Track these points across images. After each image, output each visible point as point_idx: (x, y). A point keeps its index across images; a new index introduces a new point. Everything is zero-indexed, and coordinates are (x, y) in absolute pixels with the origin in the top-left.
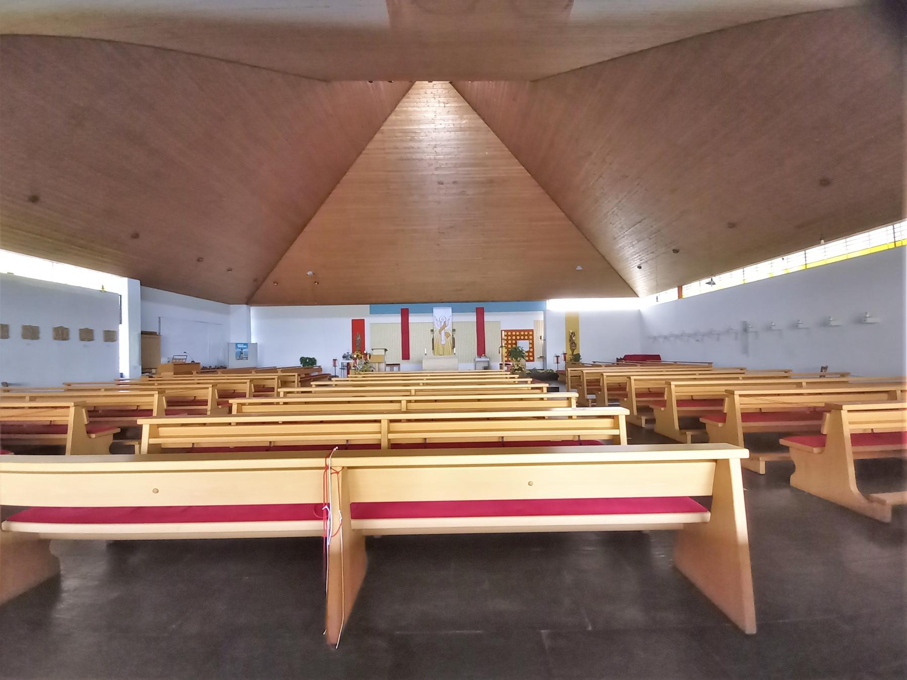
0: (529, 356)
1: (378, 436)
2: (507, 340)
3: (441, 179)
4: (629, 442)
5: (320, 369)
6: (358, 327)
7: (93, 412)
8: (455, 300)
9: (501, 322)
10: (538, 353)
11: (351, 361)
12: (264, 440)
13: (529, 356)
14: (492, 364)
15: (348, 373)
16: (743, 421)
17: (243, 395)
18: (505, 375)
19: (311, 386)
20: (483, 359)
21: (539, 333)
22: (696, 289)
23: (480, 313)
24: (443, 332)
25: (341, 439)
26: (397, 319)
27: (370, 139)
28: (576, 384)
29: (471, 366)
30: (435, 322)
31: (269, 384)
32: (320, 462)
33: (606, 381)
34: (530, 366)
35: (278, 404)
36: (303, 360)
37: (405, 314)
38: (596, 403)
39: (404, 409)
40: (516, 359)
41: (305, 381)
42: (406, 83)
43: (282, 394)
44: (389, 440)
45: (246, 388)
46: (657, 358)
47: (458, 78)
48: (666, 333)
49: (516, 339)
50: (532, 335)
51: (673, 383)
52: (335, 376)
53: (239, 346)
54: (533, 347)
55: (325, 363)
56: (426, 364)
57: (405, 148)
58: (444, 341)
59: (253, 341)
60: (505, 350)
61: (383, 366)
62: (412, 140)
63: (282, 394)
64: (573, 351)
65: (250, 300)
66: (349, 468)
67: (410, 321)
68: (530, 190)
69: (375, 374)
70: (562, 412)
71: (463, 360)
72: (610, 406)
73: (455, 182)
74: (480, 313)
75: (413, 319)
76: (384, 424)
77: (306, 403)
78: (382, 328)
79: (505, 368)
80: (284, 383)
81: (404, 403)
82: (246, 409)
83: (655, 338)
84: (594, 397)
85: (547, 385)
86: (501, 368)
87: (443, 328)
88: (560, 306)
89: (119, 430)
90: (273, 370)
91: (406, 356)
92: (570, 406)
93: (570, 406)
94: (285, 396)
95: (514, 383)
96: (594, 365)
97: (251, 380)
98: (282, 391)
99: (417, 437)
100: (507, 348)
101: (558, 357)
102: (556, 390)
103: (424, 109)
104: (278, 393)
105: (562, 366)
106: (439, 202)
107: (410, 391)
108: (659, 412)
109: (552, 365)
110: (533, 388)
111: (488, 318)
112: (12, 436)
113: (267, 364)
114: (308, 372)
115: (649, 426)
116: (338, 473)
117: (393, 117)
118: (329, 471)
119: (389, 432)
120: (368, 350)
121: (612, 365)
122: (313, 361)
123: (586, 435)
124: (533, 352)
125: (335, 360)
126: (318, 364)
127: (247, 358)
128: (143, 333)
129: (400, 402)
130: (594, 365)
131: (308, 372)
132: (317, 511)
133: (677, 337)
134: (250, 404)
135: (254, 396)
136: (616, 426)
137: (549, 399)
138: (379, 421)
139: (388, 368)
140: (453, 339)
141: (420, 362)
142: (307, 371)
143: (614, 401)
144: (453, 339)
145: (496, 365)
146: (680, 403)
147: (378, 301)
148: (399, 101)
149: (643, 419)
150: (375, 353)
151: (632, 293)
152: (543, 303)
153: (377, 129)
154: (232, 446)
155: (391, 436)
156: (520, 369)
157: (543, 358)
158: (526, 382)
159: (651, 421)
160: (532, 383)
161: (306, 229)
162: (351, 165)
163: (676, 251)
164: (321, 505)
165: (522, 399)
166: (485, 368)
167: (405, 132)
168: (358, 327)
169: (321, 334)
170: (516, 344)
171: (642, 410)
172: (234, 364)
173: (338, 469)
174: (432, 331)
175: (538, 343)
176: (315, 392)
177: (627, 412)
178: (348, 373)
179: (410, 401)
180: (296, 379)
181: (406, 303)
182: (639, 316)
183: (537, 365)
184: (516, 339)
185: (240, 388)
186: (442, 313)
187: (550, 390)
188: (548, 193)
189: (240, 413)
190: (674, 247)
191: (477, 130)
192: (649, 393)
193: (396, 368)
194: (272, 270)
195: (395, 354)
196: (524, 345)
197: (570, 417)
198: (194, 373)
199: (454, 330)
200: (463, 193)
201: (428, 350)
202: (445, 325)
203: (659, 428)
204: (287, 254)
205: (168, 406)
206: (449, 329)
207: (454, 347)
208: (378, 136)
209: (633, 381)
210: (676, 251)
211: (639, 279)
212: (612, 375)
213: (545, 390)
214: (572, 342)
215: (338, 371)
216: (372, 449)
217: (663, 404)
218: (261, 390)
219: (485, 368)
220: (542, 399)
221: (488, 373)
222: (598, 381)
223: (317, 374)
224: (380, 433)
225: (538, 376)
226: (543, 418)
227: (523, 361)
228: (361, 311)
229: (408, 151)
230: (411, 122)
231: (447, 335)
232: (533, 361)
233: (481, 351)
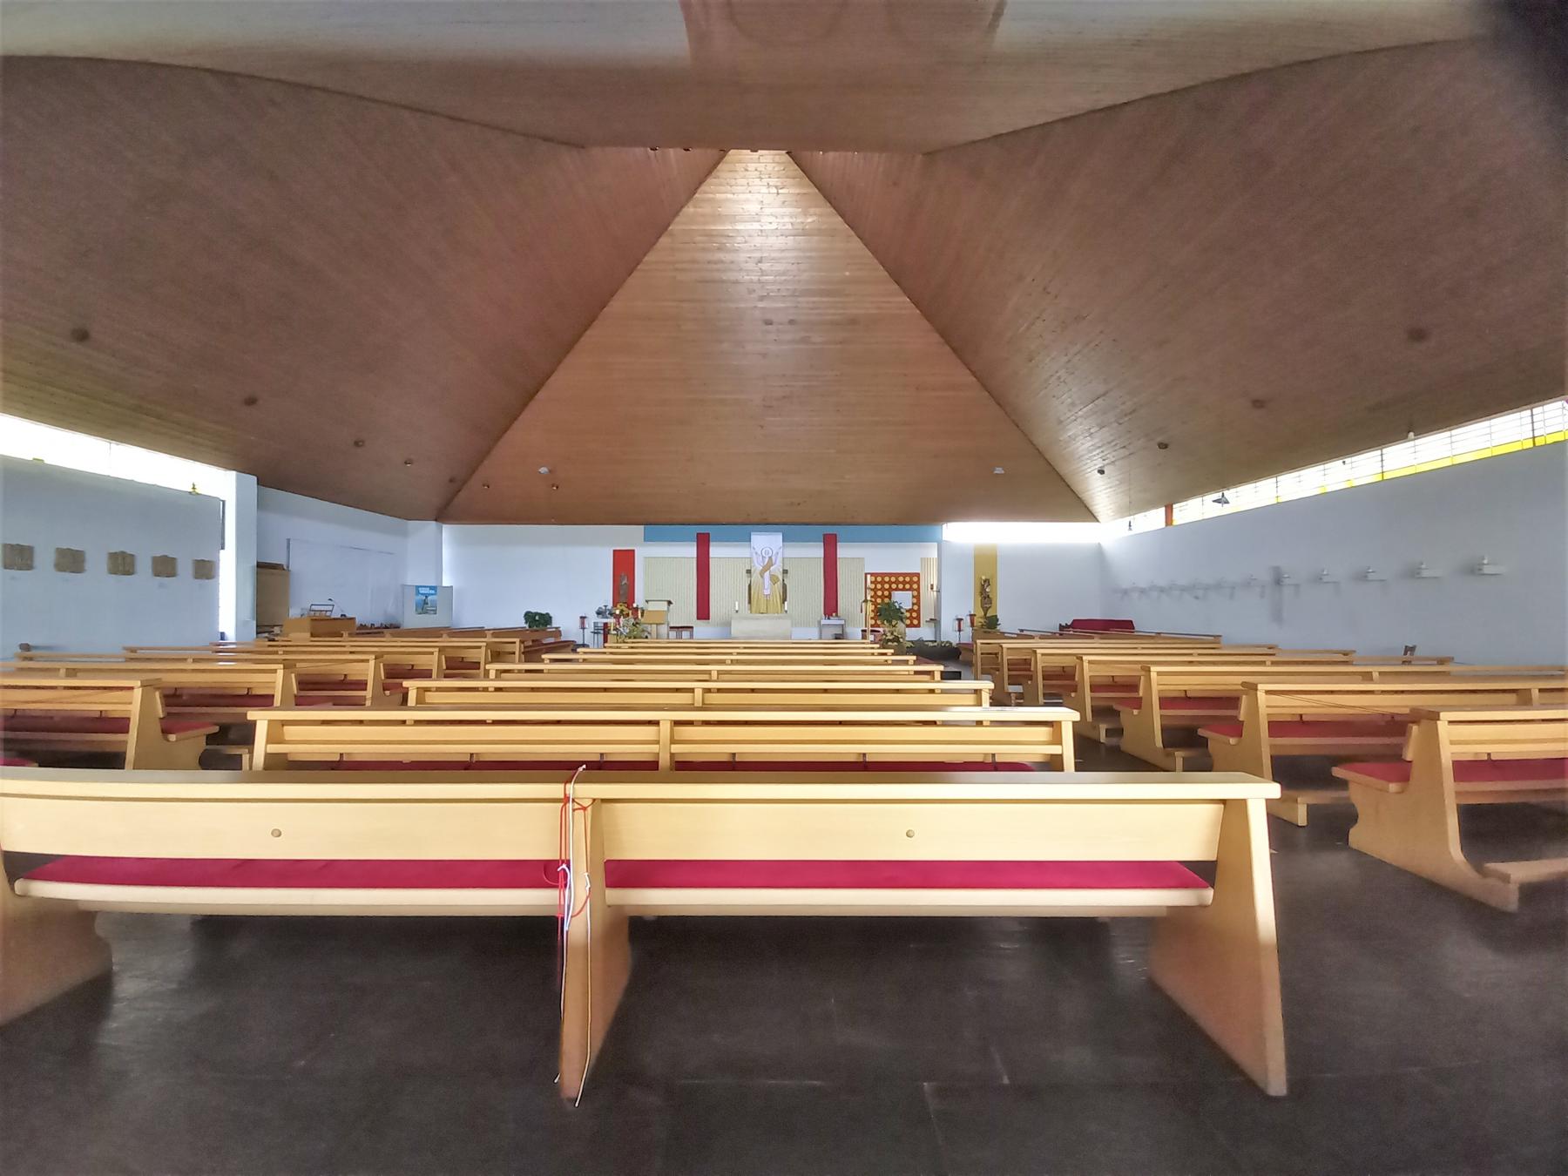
0: (911, 618)
1: (655, 748)
2: (875, 590)
3: (768, 316)
4: (1078, 768)
5: (558, 632)
6: (624, 563)
7: (173, 698)
8: (790, 523)
9: (865, 559)
10: (926, 614)
11: (611, 621)
12: (460, 751)
13: (911, 618)
14: (848, 630)
15: (605, 641)
16: (1271, 735)
17: (426, 674)
18: (870, 649)
19: (542, 661)
20: (833, 621)
21: (930, 578)
22: (1196, 510)
23: (830, 544)
25: (592, 752)
26: (691, 551)
28: (990, 668)
29: (812, 634)
30: (754, 557)
31: (471, 656)
32: (555, 790)
33: (1041, 663)
34: (912, 634)
35: (485, 689)
36: (530, 617)
37: (703, 543)
38: (1023, 700)
39: (698, 703)
40: (890, 622)
41: (532, 653)
43: (492, 674)
44: (672, 755)
45: (432, 661)
48: (1143, 585)
49: (890, 589)
50: (918, 583)
51: (1153, 669)
52: (584, 645)
53: (422, 591)
54: (918, 604)
55: (566, 623)
56: (738, 628)
58: (767, 588)
59: (445, 584)
60: (870, 607)
61: (664, 629)
63: (492, 674)
65: (443, 515)
66: (604, 801)
68: (920, 338)
69: (651, 642)
70: (966, 714)
71: (801, 622)
72: (1046, 705)
73: (792, 322)
74: (830, 544)
75: (715, 551)
76: (665, 728)
77: (533, 690)
78: (665, 566)
79: (871, 637)
80: (497, 656)
81: (698, 693)
82: (431, 697)
83: (1125, 592)
84: (1019, 689)
85: (941, 668)
86: (864, 637)
87: (766, 568)
88: (965, 534)
89: (216, 729)
90: (479, 632)
91: (703, 612)
92: (979, 704)
93: (979, 704)
95: (886, 663)
96: (1022, 635)
97: (442, 650)
98: (493, 668)
99: (721, 752)
100: (875, 603)
101: (960, 620)
102: (957, 676)
103: (742, 197)
104: (487, 672)
105: (967, 636)
106: (764, 355)
107: (709, 672)
108: (1129, 717)
109: (950, 635)
110: (916, 673)
111: (844, 552)
113: (468, 622)
114: (538, 637)
115: (1114, 741)
116: (585, 809)
117: (689, 209)
118: (570, 805)
119: (673, 741)
120: (639, 601)
121: (1052, 636)
122: (546, 619)
123: (1005, 753)
124: (918, 612)
125: (583, 618)
128: (260, 565)
129: (692, 690)
130: (1022, 635)
131: (538, 637)
133: (1162, 590)
134: (439, 689)
135: (446, 676)
136: (1057, 740)
137: (944, 692)
138: (656, 723)
139: (673, 634)
140: (784, 587)
141: (728, 624)
142: (536, 636)
143: (1053, 699)
144: (784, 587)
145: (855, 631)
146: (1166, 702)
147: (658, 519)
148: (701, 183)
149: (1103, 728)
150: (651, 607)
151: (1090, 515)
152: (937, 528)
153: (663, 229)
154: (406, 759)
155: (676, 748)
156: (896, 639)
157: (935, 621)
158: (906, 662)
159: (1116, 732)
160: (915, 663)
161: (541, 395)
163: (1163, 446)
164: (556, 863)
165: (898, 691)
166: (837, 637)
167: (709, 235)
168: (624, 563)
169: (564, 576)
170: (890, 597)
171: (1101, 712)
172: (412, 620)
173: (587, 803)
174: (749, 572)
175: (928, 597)
176: (550, 672)
177: (1076, 716)
178: (605, 641)
179: (708, 690)
180: (517, 648)
181: (705, 524)
183: (925, 633)
184: (890, 589)
185: (422, 662)
186: (766, 543)
187: (945, 676)
189: (421, 704)
190: (1159, 439)
191: (832, 233)
192: (1114, 685)
193: (685, 634)
195: (685, 611)
196: (903, 599)
197: (979, 723)
198: (345, 634)
199: (785, 572)
200: (805, 340)
201: (740, 603)
202: (770, 563)
203: (1127, 744)
205: (300, 689)
206: (777, 570)
207: (784, 600)
208: (664, 241)
209: (1086, 664)
210: (1163, 446)
211: (1100, 491)
212: (1050, 653)
213: (938, 676)
214: (985, 595)
215: (588, 637)
216: (643, 769)
217: (1137, 703)
218: (458, 666)
219: (837, 637)
220: (932, 691)
221: (841, 646)
222: (1027, 662)
223: (552, 640)
224: (657, 742)
225: (925, 652)
226: (934, 723)
227: (901, 626)
228: (629, 536)
230: (719, 218)
231: (774, 579)
232: (918, 626)
233: (831, 607)
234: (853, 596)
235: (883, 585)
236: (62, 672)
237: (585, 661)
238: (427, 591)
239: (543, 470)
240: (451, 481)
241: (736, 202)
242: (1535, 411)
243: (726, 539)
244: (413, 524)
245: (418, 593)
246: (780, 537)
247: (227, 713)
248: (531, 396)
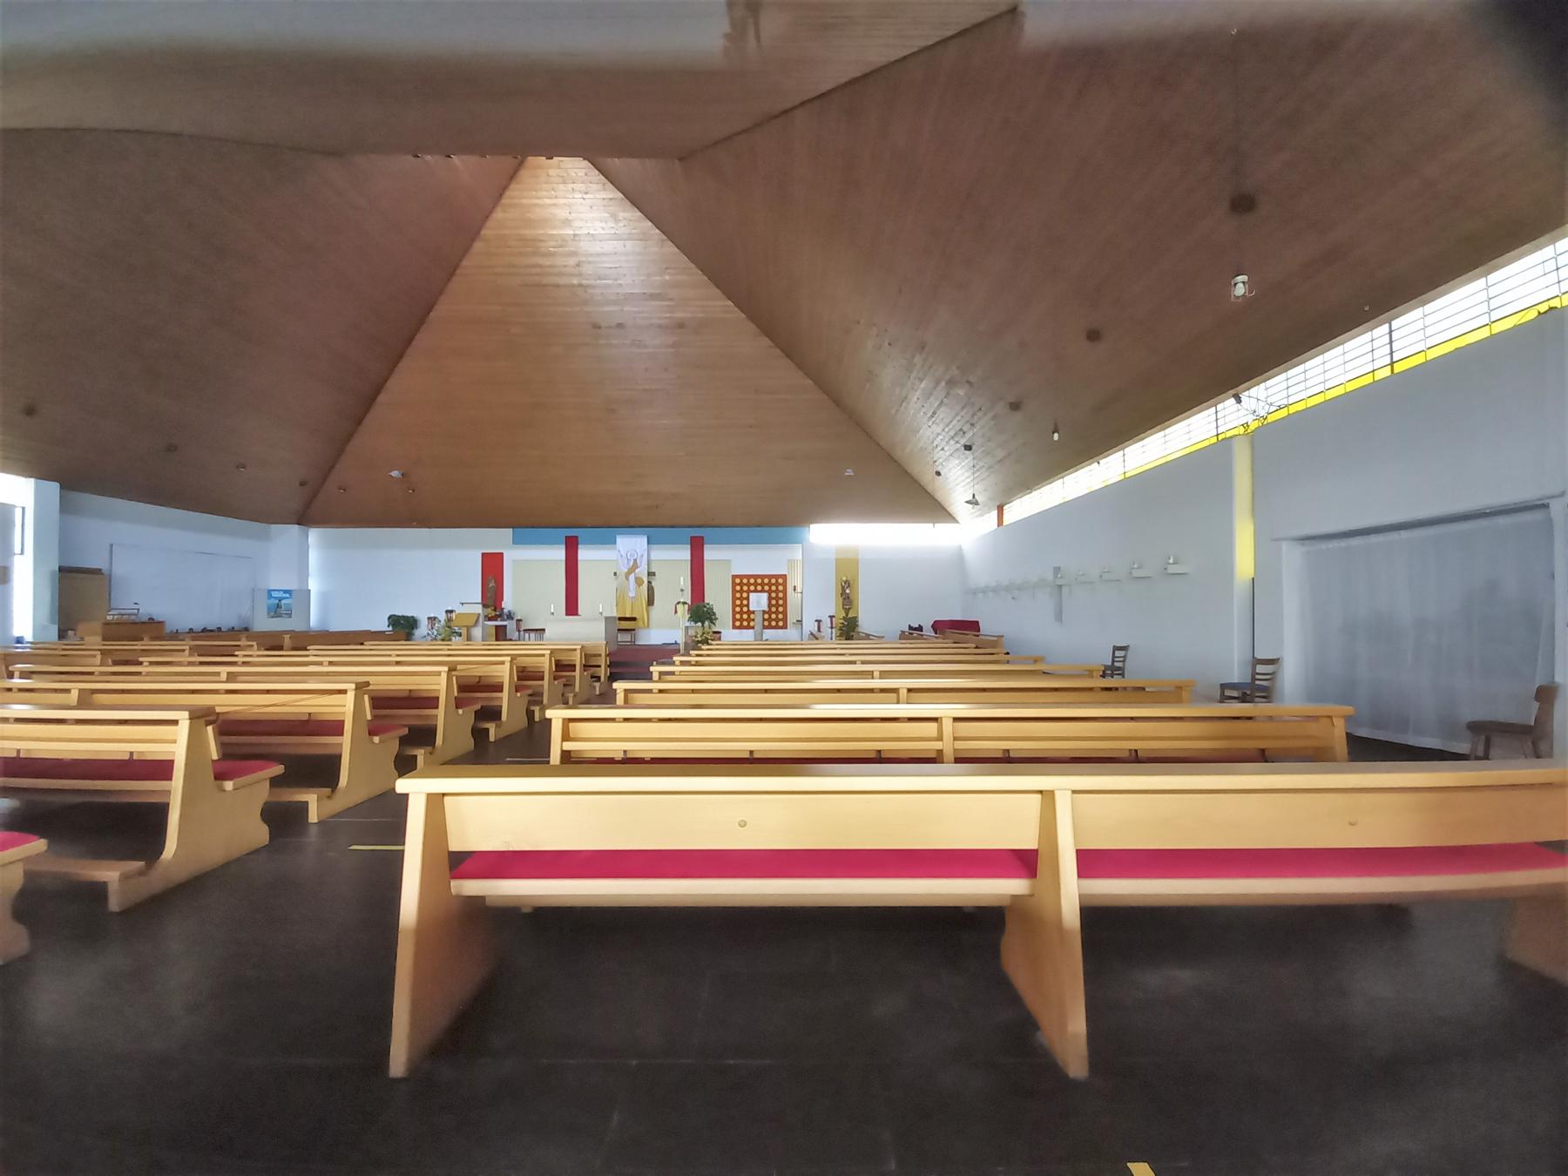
1: (938, 745)
6: (492, 566)
8: (654, 522)
9: (730, 560)
19: (673, 664)
21: (795, 580)
22: (1023, 508)
23: (697, 546)
24: (632, 577)
26: (559, 553)
27: (466, 250)
35: (649, 691)
37: (572, 546)
42: (507, 161)
46: (973, 626)
47: (598, 148)
53: (275, 594)
57: (528, 266)
62: (536, 253)
63: (656, 676)
64: (847, 611)
65: (305, 519)
67: (706, 557)
68: (750, 343)
74: (697, 546)
75: (584, 554)
78: (534, 568)
88: (830, 536)
94: (660, 680)
97: (513, 657)
101: (819, 621)
103: (562, 201)
107: (218, 674)
111: (710, 554)
112: (254, 739)
117: (498, 214)
119: (955, 739)
120: (508, 604)
126: (985, 628)
127: (290, 615)
128: (61, 569)
132: (1024, 862)
147: (528, 521)
148: (505, 188)
153: (474, 235)
154: (648, 756)
155: (961, 745)
161: (382, 398)
162: (441, 293)
167: (523, 239)
168: (492, 566)
172: (264, 623)
176: (148, 674)
182: (959, 559)
186: (631, 545)
188: (778, 346)
189: (627, 704)
190: (963, 441)
191: (644, 237)
194: (332, 467)
199: (651, 574)
204: (355, 442)
206: (642, 572)
208: (478, 246)
211: (957, 479)
214: (847, 596)
224: (940, 738)
228: (497, 539)
229: (534, 271)
230: (529, 223)
231: (639, 582)
232: (785, 627)
234: (718, 596)
235: (743, 585)
236: (876, 674)
237: (398, 663)
238: (281, 595)
239: (395, 474)
240: (302, 484)
241: (541, 206)
242: (1220, 407)
243: (594, 542)
244: (275, 528)
245: (270, 596)
246: (645, 539)
247: (412, 716)
248: (369, 401)
